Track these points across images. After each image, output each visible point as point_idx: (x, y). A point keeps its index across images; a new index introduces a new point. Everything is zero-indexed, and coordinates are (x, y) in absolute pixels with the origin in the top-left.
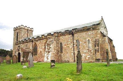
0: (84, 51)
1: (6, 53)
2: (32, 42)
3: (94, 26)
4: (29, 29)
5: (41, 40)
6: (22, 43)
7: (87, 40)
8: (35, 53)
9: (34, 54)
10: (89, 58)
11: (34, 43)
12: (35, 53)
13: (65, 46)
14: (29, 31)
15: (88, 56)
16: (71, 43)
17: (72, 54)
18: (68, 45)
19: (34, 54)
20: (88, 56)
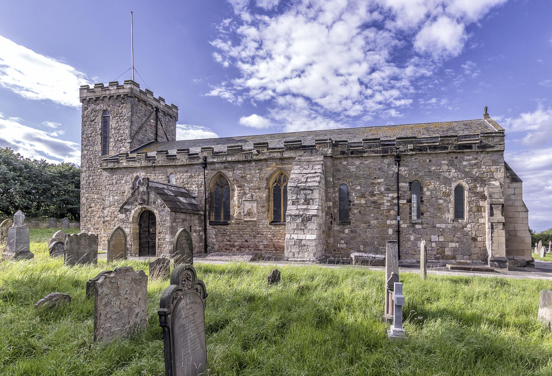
0: (438, 225)
1: (303, 228)
2: (205, 165)
3: (84, 136)
4: (161, 105)
5: (250, 162)
6: (144, 163)
7: (454, 185)
8: (217, 216)
9: (213, 219)
10: (455, 250)
11: (210, 173)
12: (217, 216)
13: (363, 202)
14: (160, 115)
15: (453, 245)
16: (388, 189)
17: (390, 231)
18: (374, 195)
19: (213, 219)
20: (453, 245)
